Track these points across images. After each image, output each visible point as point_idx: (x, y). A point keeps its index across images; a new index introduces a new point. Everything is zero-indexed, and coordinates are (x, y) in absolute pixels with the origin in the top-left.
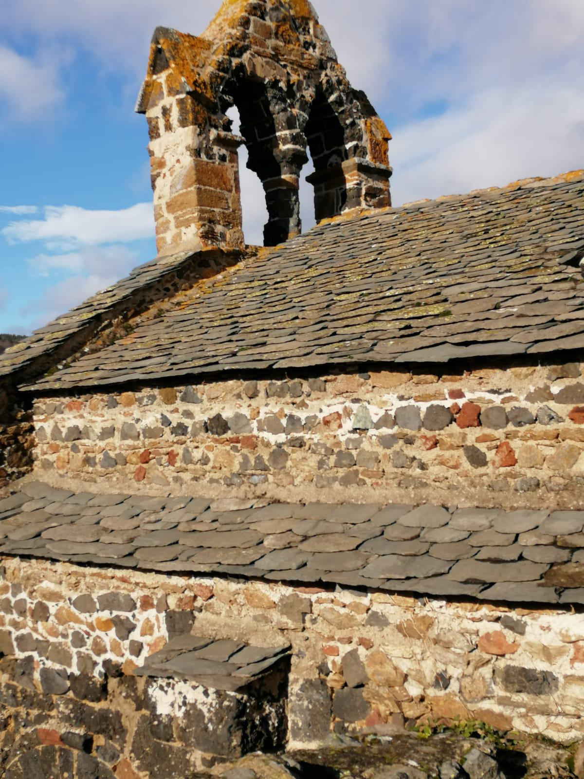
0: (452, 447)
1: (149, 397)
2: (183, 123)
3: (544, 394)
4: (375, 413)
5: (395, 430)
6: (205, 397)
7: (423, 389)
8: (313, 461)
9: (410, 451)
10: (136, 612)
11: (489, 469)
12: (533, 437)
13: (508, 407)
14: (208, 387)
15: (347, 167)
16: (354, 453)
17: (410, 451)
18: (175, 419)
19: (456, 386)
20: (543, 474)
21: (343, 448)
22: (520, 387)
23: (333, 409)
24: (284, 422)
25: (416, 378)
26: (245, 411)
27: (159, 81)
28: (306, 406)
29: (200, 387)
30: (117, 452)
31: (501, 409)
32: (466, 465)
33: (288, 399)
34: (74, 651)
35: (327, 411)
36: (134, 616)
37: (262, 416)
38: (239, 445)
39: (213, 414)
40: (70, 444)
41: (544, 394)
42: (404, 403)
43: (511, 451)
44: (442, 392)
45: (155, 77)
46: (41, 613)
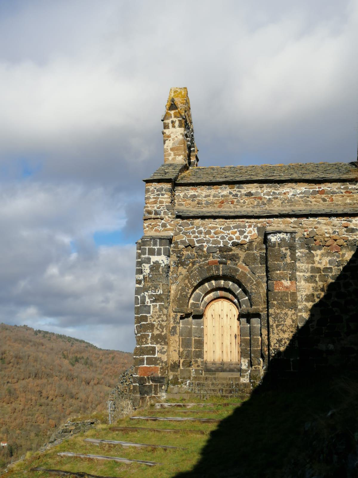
0: (319, 198)
1: (225, 187)
2: (180, 126)
3: (340, 188)
4: (299, 191)
5: (304, 195)
6: (245, 188)
7: (312, 187)
8: (280, 202)
9: (308, 199)
10: (246, 228)
11: (327, 202)
12: (338, 196)
13: (331, 191)
14: (247, 185)
15: (193, 155)
16: (293, 200)
17: (308, 199)
18: (234, 193)
19: (320, 186)
20: (340, 203)
21: (290, 199)
22: (334, 187)
23: (287, 191)
24: (272, 193)
25: (309, 185)
26: (259, 191)
27: (170, 113)
28: (279, 190)
29: (263, 178)
30: (211, 201)
31: (330, 191)
32: (322, 202)
33: (273, 188)
34: (221, 241)
35: (285, 191)
36: (246, 229)
37: (265, 192)
38: (257, 199)
39: (248, 191)
40: (191, 199)
41: (340, 188)
42: (306, 190)
43: (332, 199)
44: (316, 188)
45: (169, 111)
46: (208, 233)
